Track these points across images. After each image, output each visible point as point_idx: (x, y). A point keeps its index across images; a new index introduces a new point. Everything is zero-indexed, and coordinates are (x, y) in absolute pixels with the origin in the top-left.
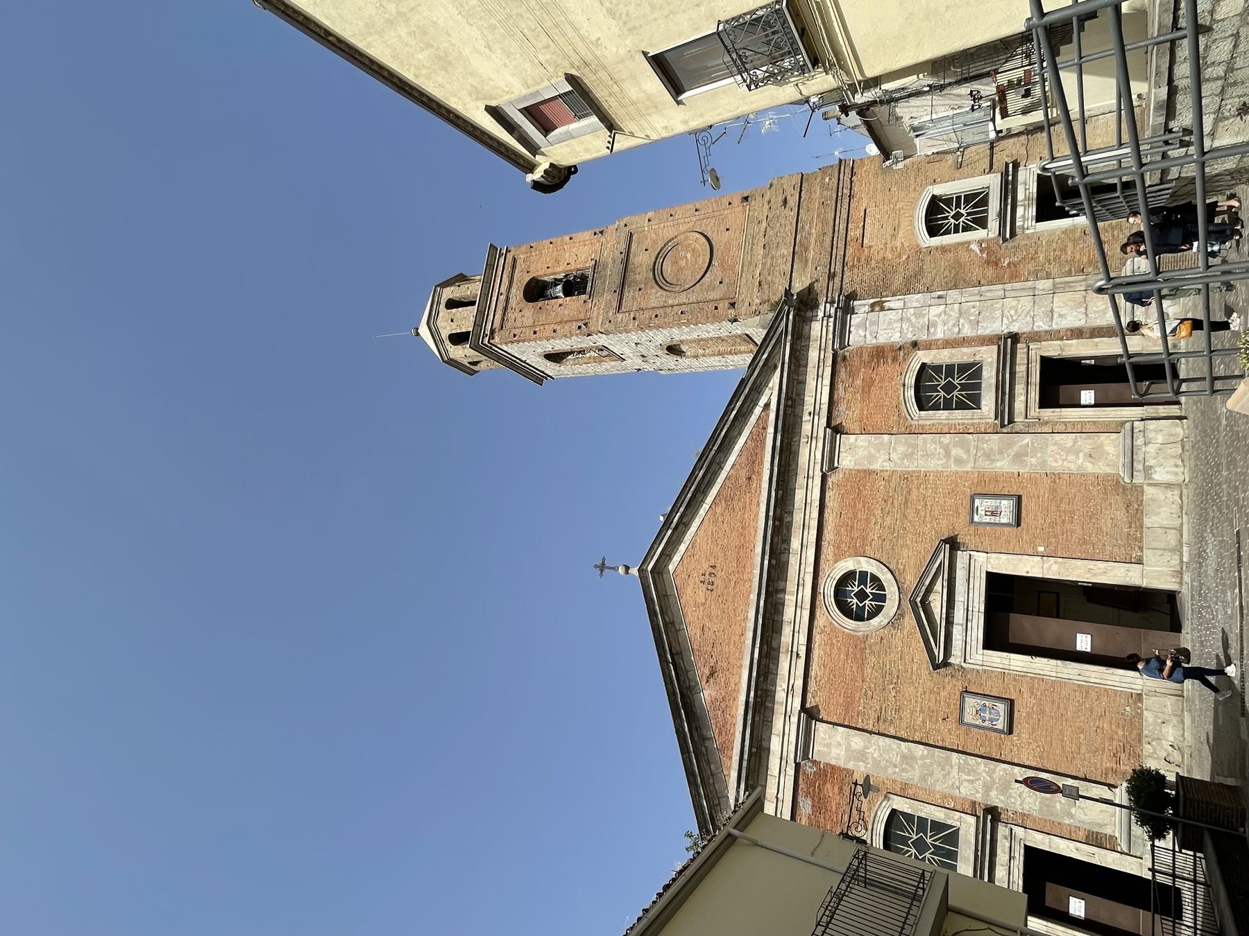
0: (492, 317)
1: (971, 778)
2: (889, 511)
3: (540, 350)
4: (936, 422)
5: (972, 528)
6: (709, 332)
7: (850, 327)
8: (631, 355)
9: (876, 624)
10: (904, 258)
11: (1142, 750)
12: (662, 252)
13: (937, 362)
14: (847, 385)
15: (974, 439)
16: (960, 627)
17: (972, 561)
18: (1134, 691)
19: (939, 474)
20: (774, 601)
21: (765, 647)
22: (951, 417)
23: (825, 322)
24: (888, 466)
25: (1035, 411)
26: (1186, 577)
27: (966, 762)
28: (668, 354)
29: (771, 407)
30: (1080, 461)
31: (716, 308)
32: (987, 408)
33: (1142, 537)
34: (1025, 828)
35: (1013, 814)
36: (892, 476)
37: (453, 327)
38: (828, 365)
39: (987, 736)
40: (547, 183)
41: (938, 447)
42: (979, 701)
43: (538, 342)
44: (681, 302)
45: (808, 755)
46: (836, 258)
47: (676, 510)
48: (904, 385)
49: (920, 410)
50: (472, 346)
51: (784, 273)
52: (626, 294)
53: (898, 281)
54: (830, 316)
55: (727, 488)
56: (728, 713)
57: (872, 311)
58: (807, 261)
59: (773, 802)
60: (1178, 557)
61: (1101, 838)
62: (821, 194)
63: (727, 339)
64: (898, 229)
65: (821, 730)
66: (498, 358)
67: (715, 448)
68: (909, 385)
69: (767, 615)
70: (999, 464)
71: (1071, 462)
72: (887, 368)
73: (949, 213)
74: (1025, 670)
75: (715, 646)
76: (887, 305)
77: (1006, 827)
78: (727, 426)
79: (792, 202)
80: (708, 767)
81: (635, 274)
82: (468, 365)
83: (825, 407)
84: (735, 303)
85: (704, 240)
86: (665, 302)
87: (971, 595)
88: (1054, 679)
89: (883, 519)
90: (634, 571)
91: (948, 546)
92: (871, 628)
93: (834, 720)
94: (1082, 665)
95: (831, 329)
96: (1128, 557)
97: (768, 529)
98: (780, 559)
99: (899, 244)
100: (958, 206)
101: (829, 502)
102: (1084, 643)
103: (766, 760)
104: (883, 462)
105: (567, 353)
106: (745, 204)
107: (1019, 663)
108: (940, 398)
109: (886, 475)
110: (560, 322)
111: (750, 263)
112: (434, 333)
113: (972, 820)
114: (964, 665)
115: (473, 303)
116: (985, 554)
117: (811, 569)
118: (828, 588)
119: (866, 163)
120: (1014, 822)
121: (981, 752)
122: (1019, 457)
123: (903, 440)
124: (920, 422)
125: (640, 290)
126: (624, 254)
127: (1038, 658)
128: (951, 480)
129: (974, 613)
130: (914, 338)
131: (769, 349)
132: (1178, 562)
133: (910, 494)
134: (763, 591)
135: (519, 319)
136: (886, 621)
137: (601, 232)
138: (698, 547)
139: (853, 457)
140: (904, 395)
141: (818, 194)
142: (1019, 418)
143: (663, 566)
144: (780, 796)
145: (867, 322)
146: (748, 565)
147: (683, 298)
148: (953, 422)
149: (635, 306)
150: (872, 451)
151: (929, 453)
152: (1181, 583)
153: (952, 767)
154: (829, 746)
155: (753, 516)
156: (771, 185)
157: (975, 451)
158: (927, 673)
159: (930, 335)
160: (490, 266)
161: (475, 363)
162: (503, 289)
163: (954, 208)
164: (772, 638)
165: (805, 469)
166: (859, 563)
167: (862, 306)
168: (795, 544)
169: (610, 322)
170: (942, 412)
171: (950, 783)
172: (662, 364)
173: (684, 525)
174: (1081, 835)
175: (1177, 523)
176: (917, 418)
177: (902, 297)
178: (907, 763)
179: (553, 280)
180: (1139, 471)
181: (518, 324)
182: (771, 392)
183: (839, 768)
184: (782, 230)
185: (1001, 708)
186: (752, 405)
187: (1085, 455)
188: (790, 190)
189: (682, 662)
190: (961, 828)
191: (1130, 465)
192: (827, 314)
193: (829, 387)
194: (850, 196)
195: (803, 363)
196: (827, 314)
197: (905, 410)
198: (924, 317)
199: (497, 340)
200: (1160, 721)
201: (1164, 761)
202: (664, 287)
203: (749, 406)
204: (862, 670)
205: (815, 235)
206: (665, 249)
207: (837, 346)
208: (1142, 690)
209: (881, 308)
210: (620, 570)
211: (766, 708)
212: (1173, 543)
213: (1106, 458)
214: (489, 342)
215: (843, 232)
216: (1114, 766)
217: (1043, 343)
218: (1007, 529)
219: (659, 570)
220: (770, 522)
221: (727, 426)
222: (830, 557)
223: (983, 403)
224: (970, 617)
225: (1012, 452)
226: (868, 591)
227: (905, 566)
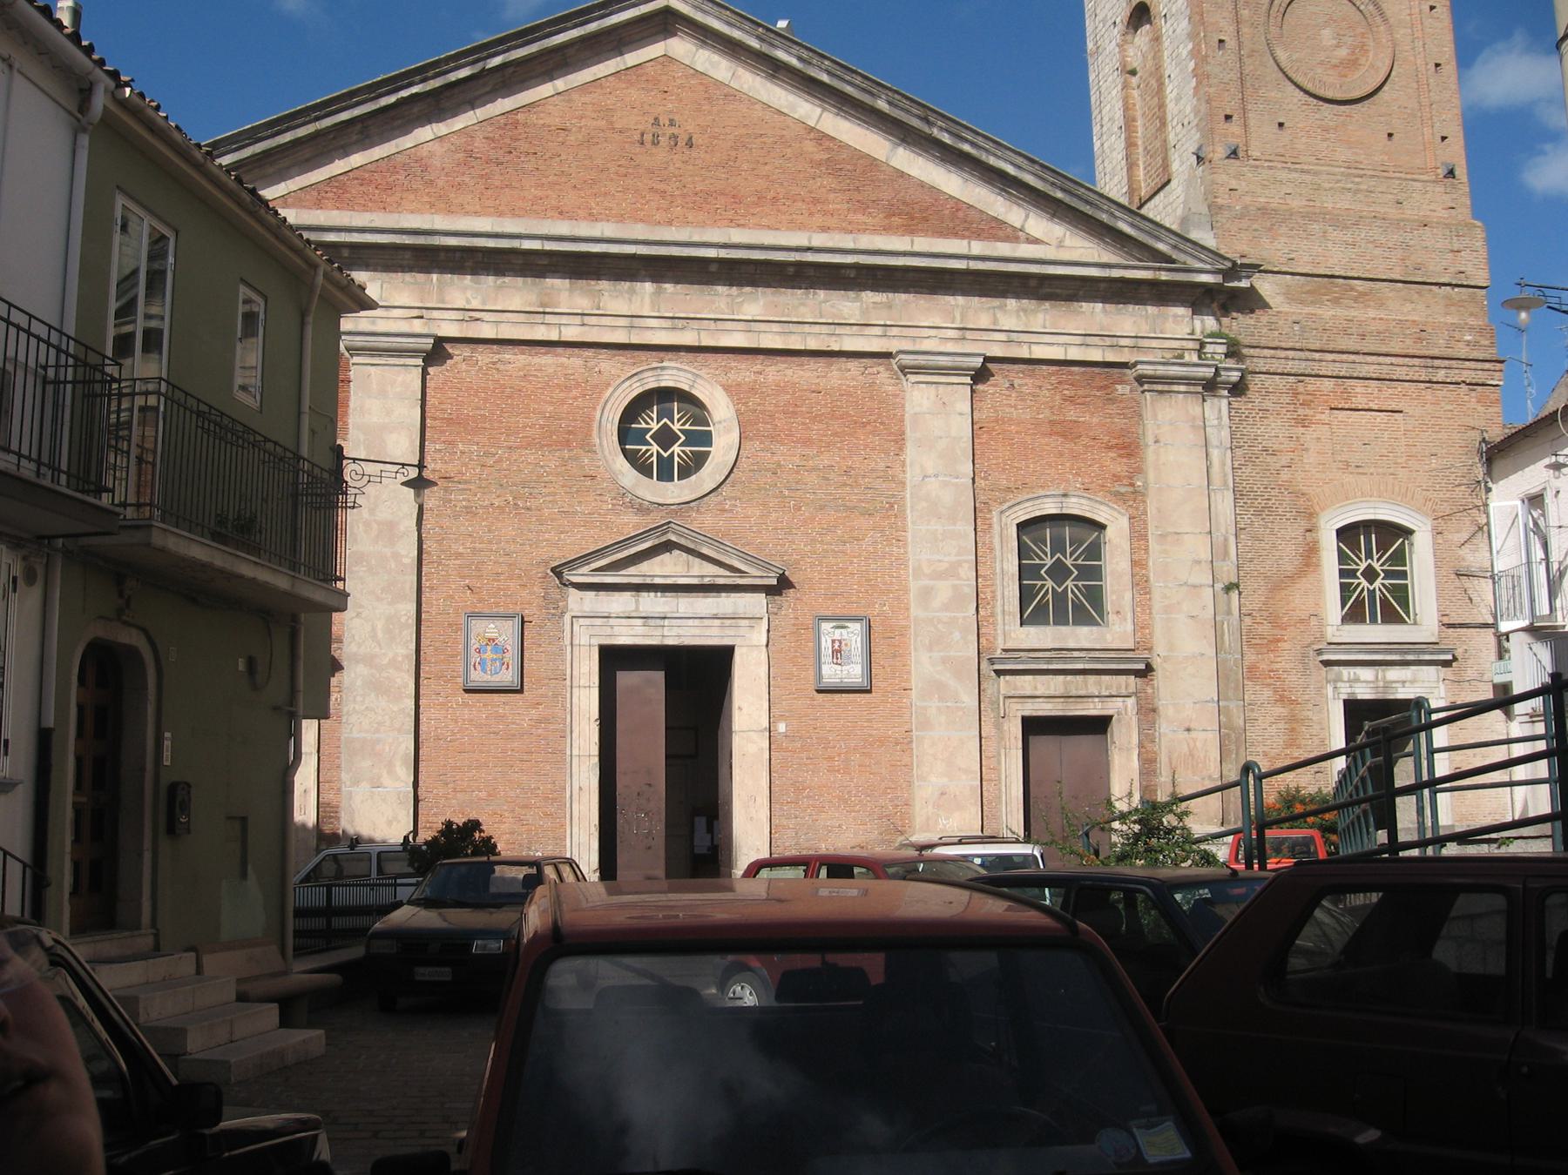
1: (380, 635)
2: (827, 479)
4: (998, 553)
13: (1107, 551)
19: (902, 562)
21: (545, 262)
22: (1006, 579)
32: (1023, 636)
41: (953, 559)
48: (1065, 495)
61: (332, 823)
73: (1378, 560)
88: (568, 753)
92: (609, 458)
93: (430, 401)
100: (1388, 574)
108: (1041, 559)
114: (567, 618)
116: (765, 643)
118: (674, 375)
124: (996, 527)
128: (892, 583)
133: (862, 514)
163: (1385, 567)
166: (728, 431)
174: (325, 797)
185: (508, 677)
189: (488, 89)
215: (1364, 371)
223: (1032, 630)
226: (676, 449)
227: (731, 511)
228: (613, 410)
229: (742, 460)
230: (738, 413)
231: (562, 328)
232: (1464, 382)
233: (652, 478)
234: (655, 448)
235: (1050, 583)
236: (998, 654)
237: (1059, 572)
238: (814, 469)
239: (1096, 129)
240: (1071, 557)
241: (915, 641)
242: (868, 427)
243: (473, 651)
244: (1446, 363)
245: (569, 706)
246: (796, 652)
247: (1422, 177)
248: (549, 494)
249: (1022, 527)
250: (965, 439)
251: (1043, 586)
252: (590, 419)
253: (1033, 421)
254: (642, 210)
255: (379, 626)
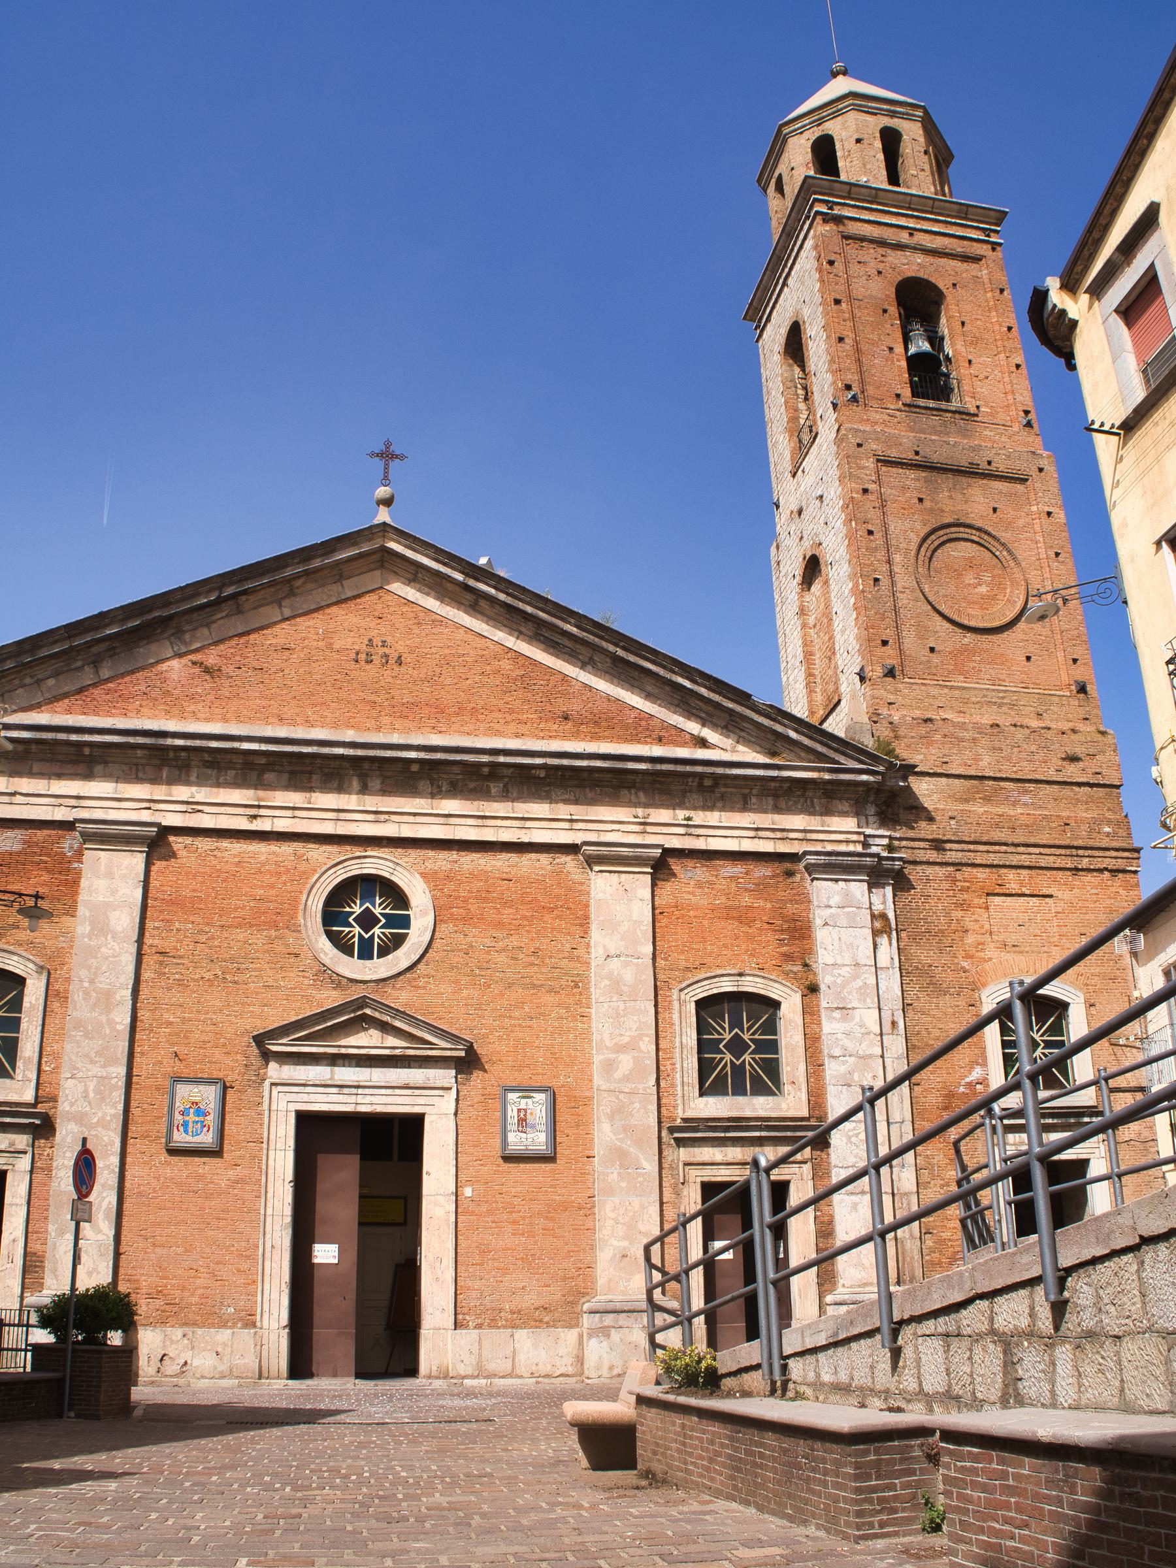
0: (867, 218)
1: (92, 1095)
2: (516, 959)
3: (806, 313)
4: (677, 1028)
5: (498, 1091)
6: (843, 632)
7: (845, 880)
8: (802, 488)
9: (320, 945)
10: (965, 964)
11: (173, 1326)
12: (990, 540)
13: (782, 1026)
14: (740, 880)
15: (649, 1088)
16: (328, 1076)
17: (440, 1092)
18: (258, 1317)
19: (586, 1035)
20: (347, 772)
21: (263, 761)
22: (685, 1052)
23: (855, 837)
24: (597, 953)
25: (698, 1176)
26: (441, 1383)
27: (114, 1088)
28: (804, 558)
29: (700, 750)
30: (615, 1243)
31: (885, 643)
32: (702, 1106)
33: (499, 1328)
34: (31, 1172)
35: (48, 1155)
36: (580, 962)
37: (846, 144)
38: (777, 846)
39: (159, 1117)
40: (1046, 315)
41: (633, 1033)
42: (212, 1106)
43: (820, 309)
44: (897, 578)
45: (91, 841)
46: (970, 851)
47: (502, 587)
48: (741, 975)
49: (696, 1002)
50: (810, 180)
51: (946, 763)
52: (912, 474)
53: (923, 955)
54: (866, 845)
55: (547, 677)
56: (144, 703)
57: (873, 916)
58: (967, 801)
59: (7, 788)
60: (470, 1373)
61: (37, 1272)
62: (1082, 821)
63: (832, 666)
64: (1014, 952)
65: (135, 861)
66: (790, 232)
67: (620, 652)
68: (740, 983)
69: (319, 761)
70: (606, 1127)
71: (613, 1230)
72: (770, 945)
73: (1038, 1031)
74: (271, 1171)
75: (257, 672)
76: (883, 940)
77: (28, 1145)
78: (661, 672)
79: (1073, 772)
80: (49, 673)
81: (950, 490)
82: (776, 175)
83: (700, 844)
84: (894, 677)
85: (1010, 615)
86: (898, 548)
87: (383, 1091)
88: (262, 1212)
89: (504, 950)
90: (383, 516)
91: (463, 1054)
92: (313, 937)
93: (154, 883)
94: (289, 1249)
95: (843, 848)
96: (465, 1310)
97: (472, 756)
98: (421, 778)
99: (988, 954)
100: (1048, 1045)
101: (527, 861)
102: (325, 1253)
103: (72, 771)
104: (604, 946)
105: (804, 366)
106: (1073, 688)
107: (280, 1163)
108: (720, 1034)
109: (581, 951)
110: (858, 350)
111: (966, 702)
112: (833, 107)
113: (29, 1096)
114: (267, 1083)
115: (893, 178)
116: (453, 1111)
117: (407, 832)
118: (376, 863)
119: (1131, 893)
120: (37, 1156)
121: (135, 1111)
122: (620, 1156)
123: (644, 977)
124: (676, 1004)
125: (921, 500)
126: (988, 467)
127: (291, 1189)
128: (576, 1056)
129: (354, 1097)
130: (823, 987)
131: (806, 741)
132: (462, 1373)
133: (549, 992)
134: (360, 752)
135: (862, 270)
136: (327, 961)
137: (1029, 424)
138: (434, 631)
139: (611, 895)
140: (723, 975)
141: (1084, 815)
142: (684, 1154)
143: (395, 569)
144: (18, 799)
145: (854, 909)
146: (407, 723)
147: (904, 580)
148: (678, 1055)
149: (889, 491)
150: (624, 928)
151: (622, 1019)
152: (429, 1377)
153: (103, 1067)
154: (110, 875)
155: (497, 726)
156: (1103, 733)
157: (627, 1090)
158: (248, 1027)
159: (829, 1013)
160: (964, 212)
161: (780, 188)
162: (921, 239)
163: (1045, 1038)
164: (281, 772)
165: (587, 815)
166: (424, 913)
167: (884, 899)
168: (451, 805)
169: (859, 445)
170: (695, 1036)
171: (79, 1065)
172: (789, 550)
173: (474, 602)
174: (35, 1247)
175: (521, 1370)
176: (683, 997)
177: (897, 964)
178: (98, 1000)
179: (940, 334)
180: (601, 1321)
181: (854, 269)
182: (729, 748)
183: (77, 893)
184: (1023, 756)
185: (207, 1139)
186: (703, 715)
187: (624, 1248)
188: (1091, 766)
189: (224, 614)
190: (13, 1082)
191: (610, 1306)
192: (871, 841)
193: (737, 849)
194: (1077, 869)
195: (782, 804)
196: (871, 841)
197: (696, 979)
198: (860, 1000)
199: (821, 228)
200: (220, 1350)
201: (163, 1352)
202: (926, 545)
203: (701, 710)
204: (239, 926)
205: (1012, 813)
206: (996, 544)
207: (811, 859)
208: (261, 1328)
209: (878, 931)
210: (383, 488)
211: (159, 768)
212: (492, 1367)
213: (621, 1278)
214: (817, 213)
215: (1015, 860)
216: (144, 1291)
217: (811, 1183)
218: (498, 1142)
219: (388, 562)
220: (485, 759)
221: (661, 672)
222: (429, 865)
223: (711, 1100)
224: (346, 1091)
225: (628, 1146)
226: (377, 931)
227: (424, 988)
228: (318, 894)
229: (437, 944)
230: (434, 898)
231: (275, 819)
232: (1106, 869)
233: (353, 957)
234: (357, 929)
235: (728, 1057)
236: (678, 1122)
237: (737, 1046)
238: (504, 950)
239: (783, 665)
240: (748, 1031)
241: (598, 1109)
242: (556, 912)
243: (177, 1113)
244: (1089, 852)
245: (264, 1167)
246: (484, 1120)
247: (1057, 693)
248: (256, 970)
249: (701, 1004)
250: (645, 923)
251: (722, 1059)
252: (296, 900)
253: (710, 906)
254: (355, 718)
255: (92, 1088)
